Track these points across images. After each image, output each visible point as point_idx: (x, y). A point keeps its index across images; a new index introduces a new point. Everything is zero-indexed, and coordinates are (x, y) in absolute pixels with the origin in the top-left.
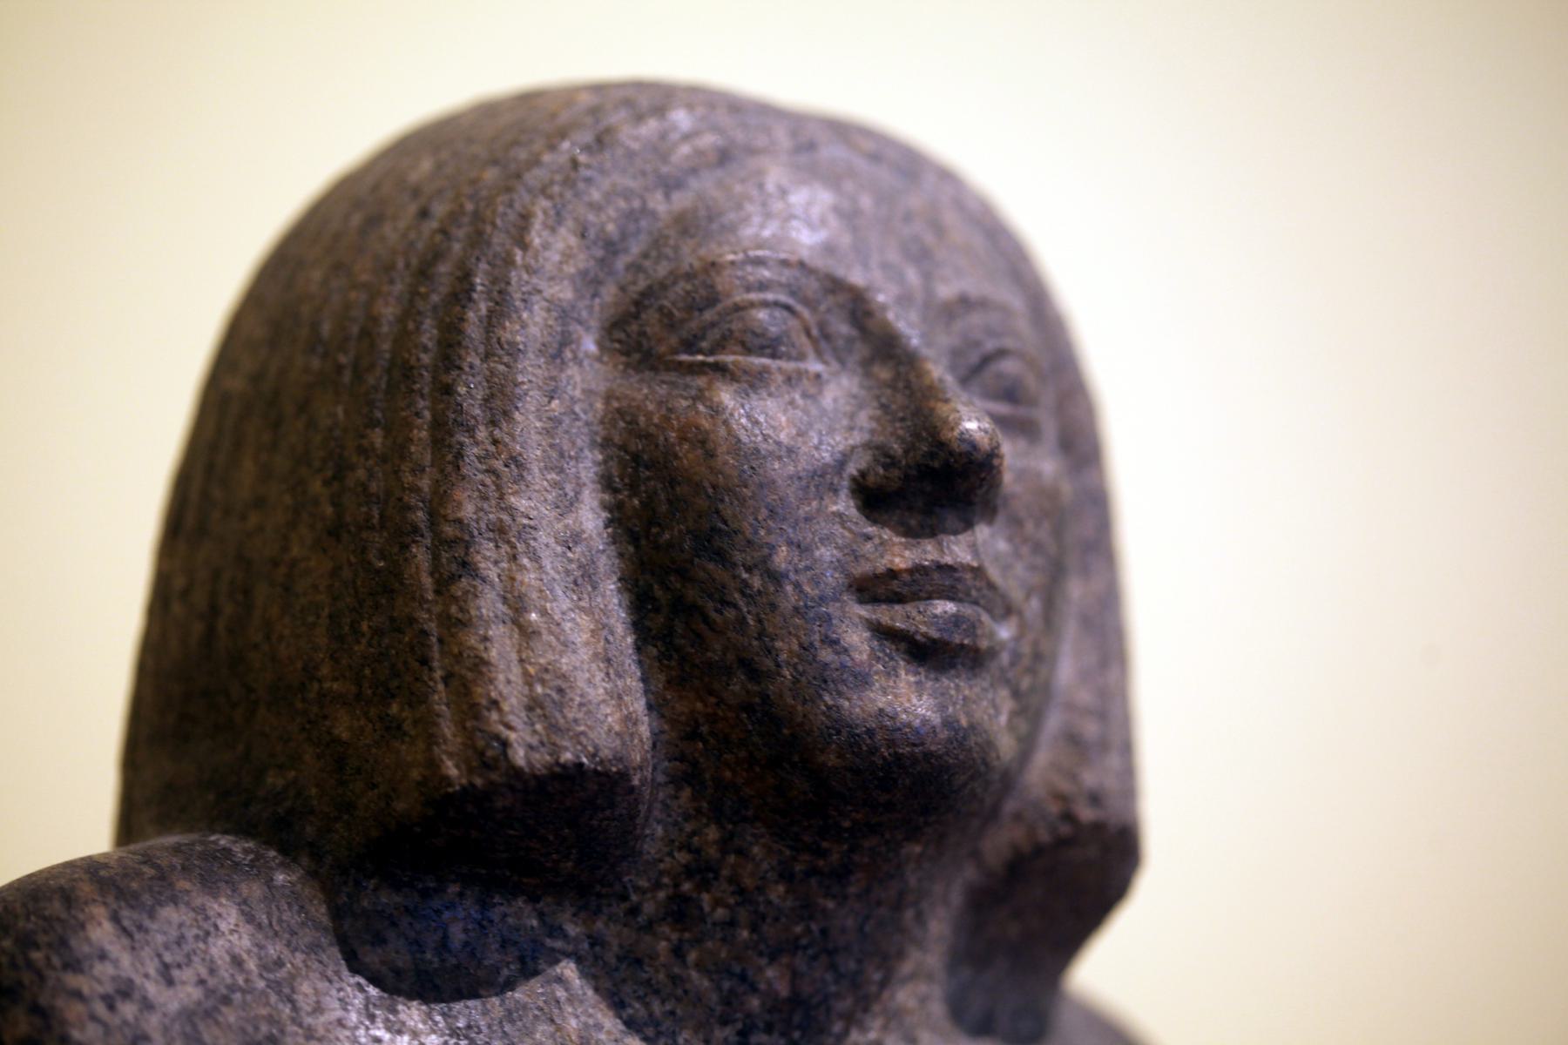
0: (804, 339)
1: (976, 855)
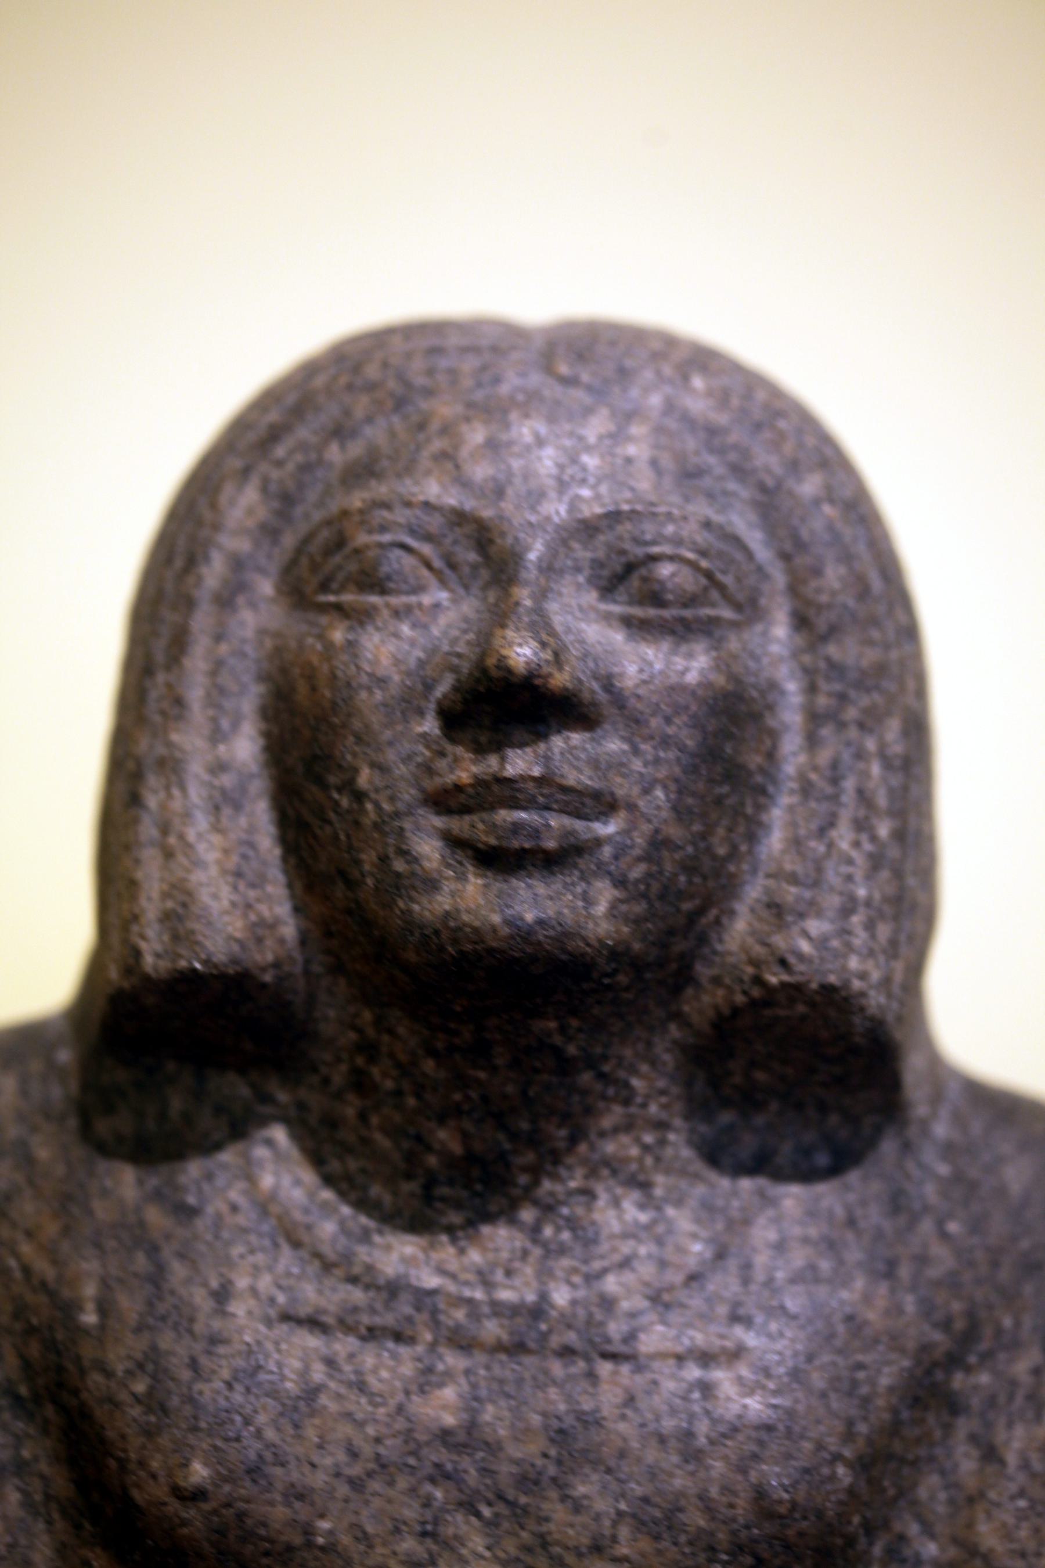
0: (425, 572)
1: (678, 1016)
